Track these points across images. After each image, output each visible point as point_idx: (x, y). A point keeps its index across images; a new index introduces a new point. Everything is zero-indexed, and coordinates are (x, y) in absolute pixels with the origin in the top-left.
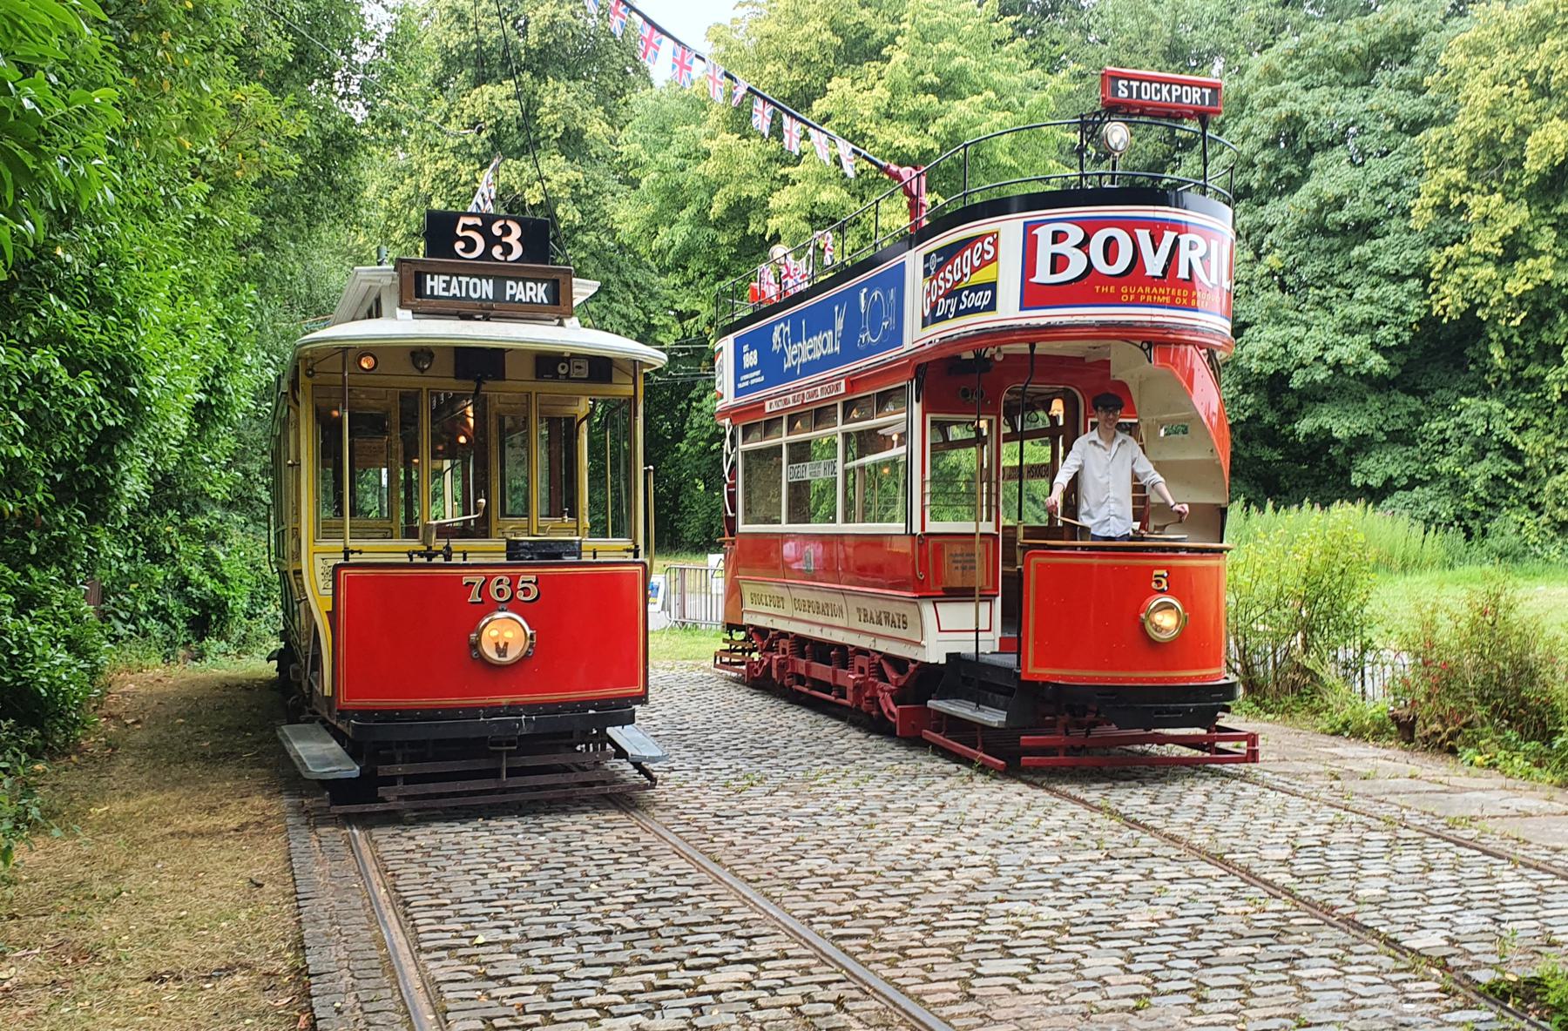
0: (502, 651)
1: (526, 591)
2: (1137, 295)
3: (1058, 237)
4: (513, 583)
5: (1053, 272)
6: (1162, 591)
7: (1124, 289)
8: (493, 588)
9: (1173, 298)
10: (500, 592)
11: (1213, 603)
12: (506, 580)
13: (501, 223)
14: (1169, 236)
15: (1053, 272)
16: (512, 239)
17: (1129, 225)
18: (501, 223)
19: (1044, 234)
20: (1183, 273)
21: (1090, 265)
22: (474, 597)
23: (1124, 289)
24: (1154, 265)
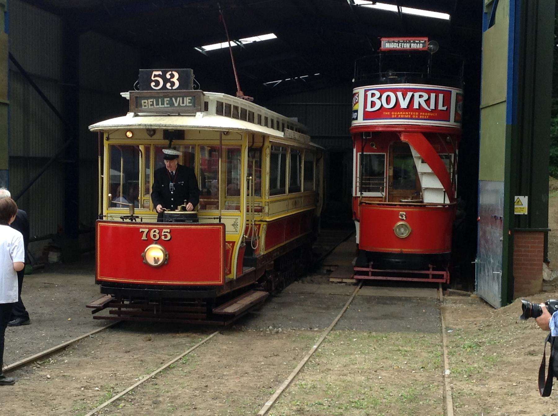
0: (156, 260)
1: (166, 236)
2: (398, 115)
3: (373, 95)
4: (161, 231)
5: (372, 107)
6: (403, 220)
7: (393, 113)
8: (152, 233)
9: (412, 116)
10: (155, 236)
11: (299, 183)
12: (157, 231)
13: (170, 73)
14: (409, 94)
15: (372, 107)
16: (175, 80)
17: (394, 91)
19: (369, 94)
20: (416, 106)
21: (382, 105)
22: (144, 238)
23: (393, 113)
24: (404, 104)
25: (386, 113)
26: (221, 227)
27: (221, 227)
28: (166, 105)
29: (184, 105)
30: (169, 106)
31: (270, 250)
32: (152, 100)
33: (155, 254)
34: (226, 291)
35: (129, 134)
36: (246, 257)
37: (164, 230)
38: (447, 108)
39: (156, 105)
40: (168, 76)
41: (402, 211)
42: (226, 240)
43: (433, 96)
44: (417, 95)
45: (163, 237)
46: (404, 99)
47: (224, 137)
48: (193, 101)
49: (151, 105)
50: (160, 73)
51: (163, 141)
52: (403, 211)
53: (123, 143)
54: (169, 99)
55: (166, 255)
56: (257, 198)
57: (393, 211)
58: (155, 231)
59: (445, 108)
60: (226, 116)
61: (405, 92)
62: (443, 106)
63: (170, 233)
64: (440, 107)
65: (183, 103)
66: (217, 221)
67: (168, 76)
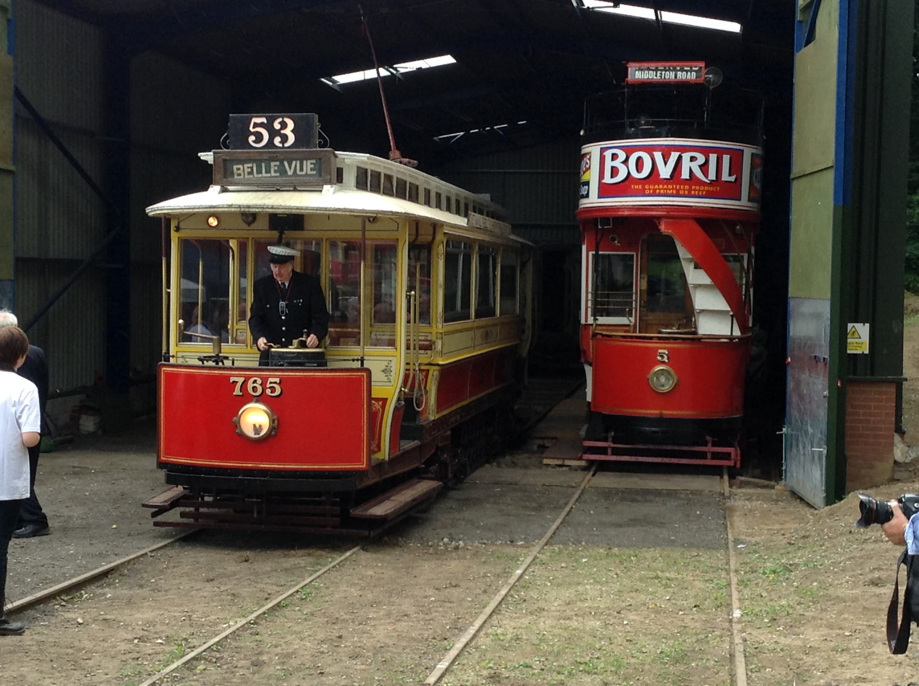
0: (257, 430)
1: (273, 389)
2: (655, 190)
3: (614, 157)
4: (264, 380)
5: (612, 177)
6: (664, 362)
7: (647, 187)
8: (250, 385)
9: (678, 191)
10: (254, 389)
11: (492, 301)
12: (259, 381)
13: (280, 120)
14: (674, 156)
15: (612, 177)
16: (288, 131)
17: (650, 150)
18: (280, 120)
19: (608, 154)
20: (685, 175)
21: (629, 173)
22: (237, 392)
23: (647, 187)
24: (665, 172)
25: (636, 187)
26: (365, 374)
27: (365, 374)
28: (273, 174)
29: (304, 173)
30: (278, 174)
31: (445, 412)
32: (250, 165)
33: (255, 418)
34: (372, 480)
35: (213, 222)
36: (405, 424)
37: (271, 380)
38: (736, 179)
39: (258, 173)
40: (277, 126)
41: (662, 348)
42: (373, 396)
43: (713, 158)
44: (686, 156)
45: (268, 392)
46: (666, 163)
47: (368, 226)
48: (317, 167)
49: (249, 173)
50: (264, 120)
51: (269, 232)
52: (664, 348)
53: (203, 236)
54: (278, 163)
55: (273, 421)
56: (423, 327)
57: (646, 348)
58: (255, 382)
59: (732, 179)
60: (371, 191)
61: (666, 152)
62: (730, 175)
63: (279, 384)
64: (725, 177)
65: (301, 170)
66: (357, 365)
67: (277, 126)
